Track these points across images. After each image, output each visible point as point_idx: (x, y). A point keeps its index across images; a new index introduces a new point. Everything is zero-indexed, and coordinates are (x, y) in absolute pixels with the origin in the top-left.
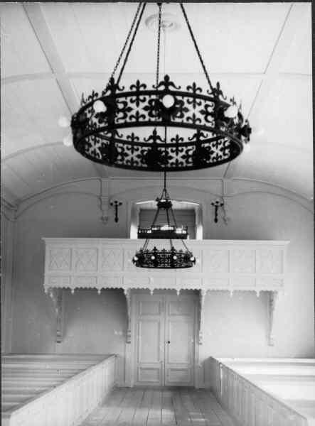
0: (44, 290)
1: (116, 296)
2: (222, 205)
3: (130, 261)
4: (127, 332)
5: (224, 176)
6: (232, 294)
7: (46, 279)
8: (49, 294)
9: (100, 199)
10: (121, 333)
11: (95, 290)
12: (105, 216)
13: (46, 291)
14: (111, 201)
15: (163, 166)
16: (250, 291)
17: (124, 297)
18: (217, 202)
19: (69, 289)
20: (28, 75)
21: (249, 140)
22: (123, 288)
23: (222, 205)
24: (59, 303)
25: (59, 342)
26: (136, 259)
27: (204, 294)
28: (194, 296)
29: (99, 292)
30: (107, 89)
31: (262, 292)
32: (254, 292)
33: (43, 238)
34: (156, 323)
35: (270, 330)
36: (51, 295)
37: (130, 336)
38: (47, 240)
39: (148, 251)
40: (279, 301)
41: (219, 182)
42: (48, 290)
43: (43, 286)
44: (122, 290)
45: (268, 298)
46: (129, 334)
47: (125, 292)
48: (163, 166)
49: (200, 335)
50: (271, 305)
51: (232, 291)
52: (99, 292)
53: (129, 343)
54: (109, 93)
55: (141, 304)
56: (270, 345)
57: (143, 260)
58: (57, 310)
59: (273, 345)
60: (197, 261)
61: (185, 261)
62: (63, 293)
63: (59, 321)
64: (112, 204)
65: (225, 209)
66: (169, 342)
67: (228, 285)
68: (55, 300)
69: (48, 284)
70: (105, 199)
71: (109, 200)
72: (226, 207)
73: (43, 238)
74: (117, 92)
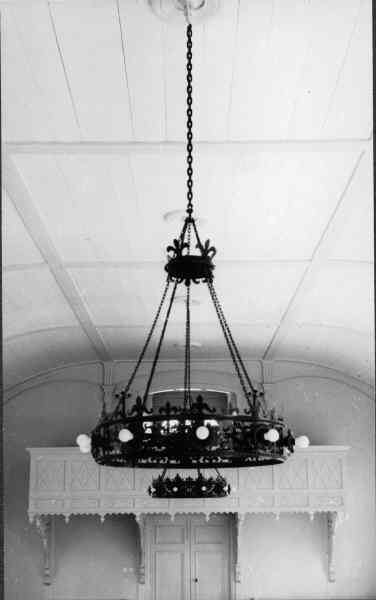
0: (28, 518)
1: (127, 526)
2: (262, 394)
3: (146, 490)
4: (139, 568)
6: (278, 518)
7: (31, 503)
8: (35, 522)
10: (131, 570)
11: (97, 516)
13: (31, 520)
14: (117, 392)
15: (195, 462)
16: (300, 513)
17: (135, 526)
19: (62, 517)
20: (15, 266)
21: (292, 451)
22: (135, 513)
23: (262, 394)
24: (48, 531)
25: (48, 584)
26: (153, 490)
27: (241, 518)
28: (231, 519)
29: (103, 520)
30: (133, 410)
31: (317, 514)
32: (307, 515)
33: (28, 449)
34: (179, 555)
35: (329, 562)
36: (38, 524)
37: (143, 574)
38: (32, 451)
39: (168, 479)
40: (338, 524)
42: (35, 517)
43: (26, 513)
44: (132, 516)
45: (326, 520)
46: (142, 571)
47: (138, 519)
48: (195, 462)
49: (237, 570)
50: (329, 527)
51: (278, 514)
52: (103, 520)
53: (143, 583)
54: (135, 413)
55: (158, 529)
56: (331, 581)
57: (161, 489)
58: (45, 543)
59: (333, 581)
60: (233, 489)
61: (218, 489)
62: (52, 522)
63: (46, 556)
64: (117, 396)
66: (196, 580)
67: (273, 505)
68: (43, 529)
69: (33, 510)
70: (108, 390)
71: (114, 390)
72: (266, 396)
73: (28, 449)
74: (145, 414)
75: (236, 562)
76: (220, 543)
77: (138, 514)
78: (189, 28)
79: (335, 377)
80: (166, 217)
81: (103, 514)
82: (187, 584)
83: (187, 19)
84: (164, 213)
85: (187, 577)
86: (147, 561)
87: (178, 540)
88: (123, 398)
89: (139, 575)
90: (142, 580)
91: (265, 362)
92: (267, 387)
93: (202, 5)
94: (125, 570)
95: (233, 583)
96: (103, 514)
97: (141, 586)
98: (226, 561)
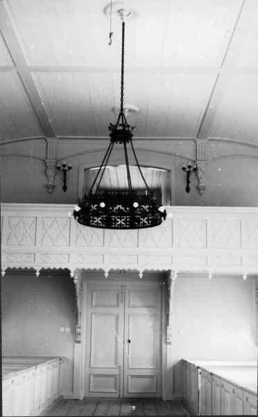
5: (197, 136)
9: (46, 163)
12: (50, 183)
18: (189, 167)
22: (69, 268)
23: (195, 170)
37: (80, 334)
41: (193, 143)
44: (67, 272)
53: (79, 342)
65: (199, 176)
66: (129, 341)
70: (51, 164)
72: (200, 173)
75: (167, 324)
76: (154, 307)
77: (72, 269)
78: (123, 24)
79: (119, 340)
80: (105, 10)
81: (38, 269)
82: (121, 346)
83: (122, 19)
84: (102, 9)
85: (120, 340)
86: (83, 321)
87: (114, 302)
88: (65, 171)
89: (75, 334)
90: (77, 339)
91: (195, 159)
92: (200, 165)
93: (129, 15)
94: (62, 329)
95: (164, 345)
96: (38, 269)
97: (77, 345)
98: (158, 324)
